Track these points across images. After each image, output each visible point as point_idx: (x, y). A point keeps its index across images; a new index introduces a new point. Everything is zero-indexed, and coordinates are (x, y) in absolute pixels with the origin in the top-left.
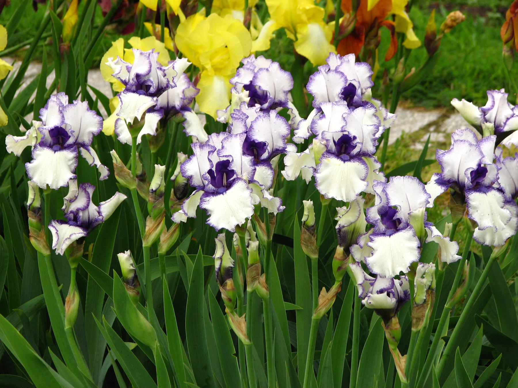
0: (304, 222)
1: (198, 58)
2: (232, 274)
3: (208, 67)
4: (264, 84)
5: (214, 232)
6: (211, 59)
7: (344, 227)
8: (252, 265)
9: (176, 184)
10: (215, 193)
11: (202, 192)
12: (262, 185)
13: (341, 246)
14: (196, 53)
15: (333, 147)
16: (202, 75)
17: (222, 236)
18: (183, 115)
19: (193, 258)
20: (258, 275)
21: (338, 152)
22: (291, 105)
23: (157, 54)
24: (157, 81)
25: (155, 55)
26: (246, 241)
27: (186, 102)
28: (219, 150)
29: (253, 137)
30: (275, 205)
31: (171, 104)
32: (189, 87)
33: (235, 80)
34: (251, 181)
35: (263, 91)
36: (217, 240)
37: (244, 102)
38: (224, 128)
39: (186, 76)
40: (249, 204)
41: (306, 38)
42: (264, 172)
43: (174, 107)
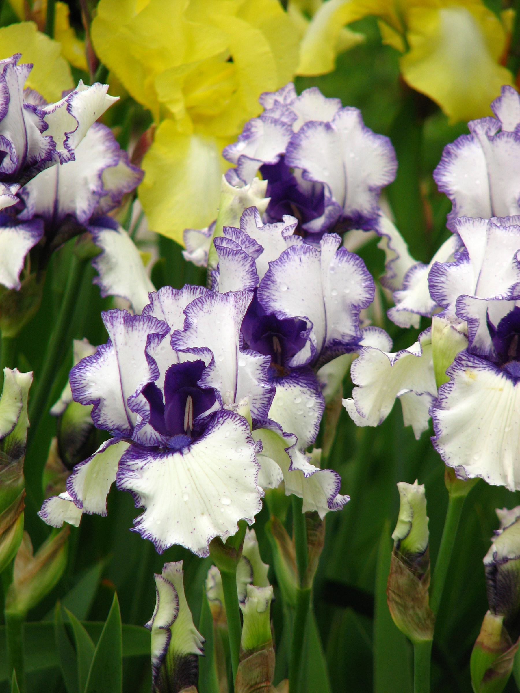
0: (400, 541)
1: (152, 87)
2: (196, 675)
3: (177, 109)
4: (316, 165)
5: (155, 557)
6: (186, 90)
7: (506, 560)
8: (251, 652)
9: (64, 426)
10: (159, 450)
11: (124, 446)
12: (289, 435)
13: (496, 612)
14: (146, 71)
15: (485, 340)
16: (158, 132)
17: (175, 568)
18: (95, 239)
19: (94, 633)
20: (267, 680)
21: (499, 354)
22: (387, 225)
23: (25, 70)
24: (21, 142)
25: (20, 70)
26: (239, 589)
27: (105, 202)
28: (177, 333)
29: (272, 304)
30: (323, 491)
31: (64, 206)
32: (116, 165)
33: (241, 148)
34: (260, 422)
35: (314, 184)
36: (159, 580)
37: (254, 209)
38: (202, 278)
39: (109, 134)
40: (251, 481)
41: (434, 47)
42: (298, 401)
43: (71, 216)
